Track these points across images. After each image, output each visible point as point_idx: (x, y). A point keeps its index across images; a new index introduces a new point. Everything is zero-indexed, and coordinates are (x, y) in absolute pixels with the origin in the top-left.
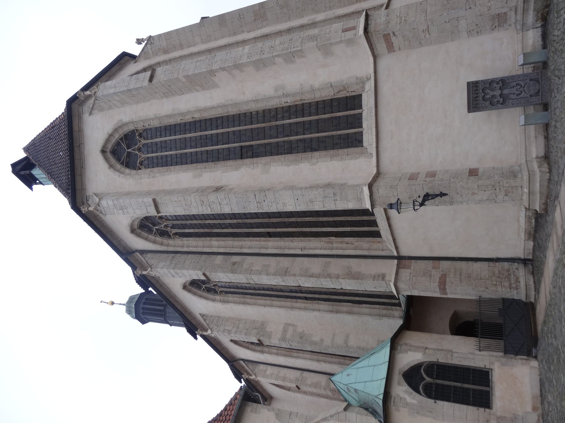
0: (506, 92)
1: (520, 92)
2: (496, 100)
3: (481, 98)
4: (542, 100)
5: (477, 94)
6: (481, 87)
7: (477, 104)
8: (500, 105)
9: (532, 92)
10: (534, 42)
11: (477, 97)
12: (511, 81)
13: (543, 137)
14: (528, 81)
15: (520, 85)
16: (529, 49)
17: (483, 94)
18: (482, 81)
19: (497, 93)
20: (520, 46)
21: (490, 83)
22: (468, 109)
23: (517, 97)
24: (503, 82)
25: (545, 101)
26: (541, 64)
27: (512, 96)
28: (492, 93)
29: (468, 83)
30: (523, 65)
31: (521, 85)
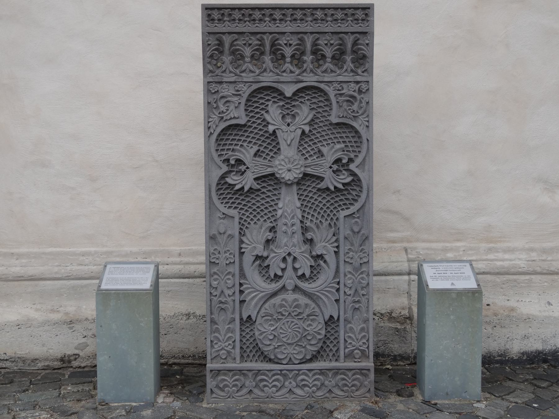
0: (289, 203)
1: (275, 270)
2: (247, 154)
3: (267, 79)
4: (217, 372)
5: (297, 59)
6: (333, 79)
7: (237, 56)
8: (217, 174)
9: (264, 329)
10: (528, 319)
11: (278, 57)
12: (344, 231)
13: (70, 351)
14: (330, 310)
15: (315, 271)
16: (496, 299)
17: (289, 91)
18: (364, 89)
19: (288, 163)
20: (520, 260)
21: (348, 130)
22: (219, 8)
23: (248, 259)
24: (342, 192)
25: (210, 383)
26: (414, 345)
27: (256, 237)
28: (288, 136)
29: (367, 11)
30: (422, 285)
31: (312, 278)
